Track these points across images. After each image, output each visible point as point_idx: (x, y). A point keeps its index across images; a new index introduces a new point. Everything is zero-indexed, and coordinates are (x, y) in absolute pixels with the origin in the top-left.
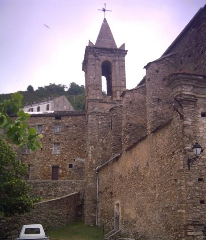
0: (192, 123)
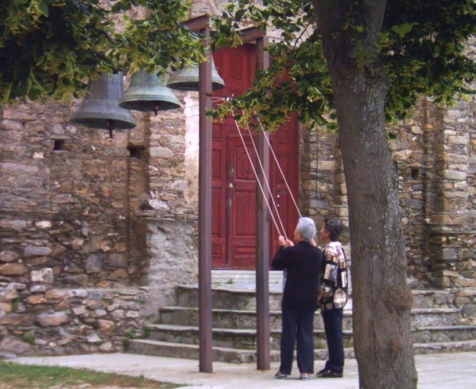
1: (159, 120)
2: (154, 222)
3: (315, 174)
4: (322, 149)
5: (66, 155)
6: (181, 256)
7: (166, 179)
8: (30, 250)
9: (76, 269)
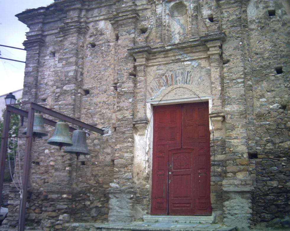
0: (33, 69)
1: (119, 147)
2: (112, 193)
3: (213, 163)
4: (218, 149)
5: (84, 167)
6: (125, 209)
7: (121, 173)
8: (58, 207)
9: (86, 214)
